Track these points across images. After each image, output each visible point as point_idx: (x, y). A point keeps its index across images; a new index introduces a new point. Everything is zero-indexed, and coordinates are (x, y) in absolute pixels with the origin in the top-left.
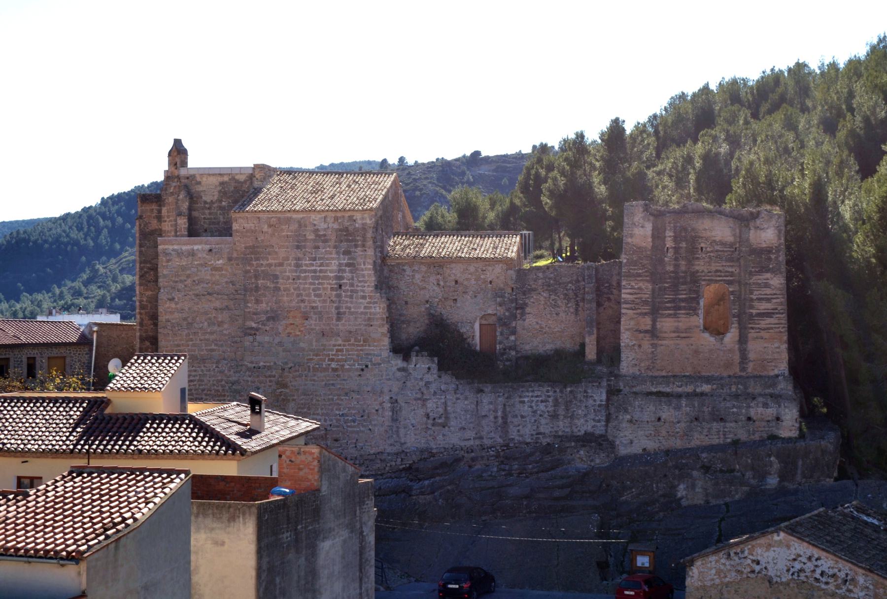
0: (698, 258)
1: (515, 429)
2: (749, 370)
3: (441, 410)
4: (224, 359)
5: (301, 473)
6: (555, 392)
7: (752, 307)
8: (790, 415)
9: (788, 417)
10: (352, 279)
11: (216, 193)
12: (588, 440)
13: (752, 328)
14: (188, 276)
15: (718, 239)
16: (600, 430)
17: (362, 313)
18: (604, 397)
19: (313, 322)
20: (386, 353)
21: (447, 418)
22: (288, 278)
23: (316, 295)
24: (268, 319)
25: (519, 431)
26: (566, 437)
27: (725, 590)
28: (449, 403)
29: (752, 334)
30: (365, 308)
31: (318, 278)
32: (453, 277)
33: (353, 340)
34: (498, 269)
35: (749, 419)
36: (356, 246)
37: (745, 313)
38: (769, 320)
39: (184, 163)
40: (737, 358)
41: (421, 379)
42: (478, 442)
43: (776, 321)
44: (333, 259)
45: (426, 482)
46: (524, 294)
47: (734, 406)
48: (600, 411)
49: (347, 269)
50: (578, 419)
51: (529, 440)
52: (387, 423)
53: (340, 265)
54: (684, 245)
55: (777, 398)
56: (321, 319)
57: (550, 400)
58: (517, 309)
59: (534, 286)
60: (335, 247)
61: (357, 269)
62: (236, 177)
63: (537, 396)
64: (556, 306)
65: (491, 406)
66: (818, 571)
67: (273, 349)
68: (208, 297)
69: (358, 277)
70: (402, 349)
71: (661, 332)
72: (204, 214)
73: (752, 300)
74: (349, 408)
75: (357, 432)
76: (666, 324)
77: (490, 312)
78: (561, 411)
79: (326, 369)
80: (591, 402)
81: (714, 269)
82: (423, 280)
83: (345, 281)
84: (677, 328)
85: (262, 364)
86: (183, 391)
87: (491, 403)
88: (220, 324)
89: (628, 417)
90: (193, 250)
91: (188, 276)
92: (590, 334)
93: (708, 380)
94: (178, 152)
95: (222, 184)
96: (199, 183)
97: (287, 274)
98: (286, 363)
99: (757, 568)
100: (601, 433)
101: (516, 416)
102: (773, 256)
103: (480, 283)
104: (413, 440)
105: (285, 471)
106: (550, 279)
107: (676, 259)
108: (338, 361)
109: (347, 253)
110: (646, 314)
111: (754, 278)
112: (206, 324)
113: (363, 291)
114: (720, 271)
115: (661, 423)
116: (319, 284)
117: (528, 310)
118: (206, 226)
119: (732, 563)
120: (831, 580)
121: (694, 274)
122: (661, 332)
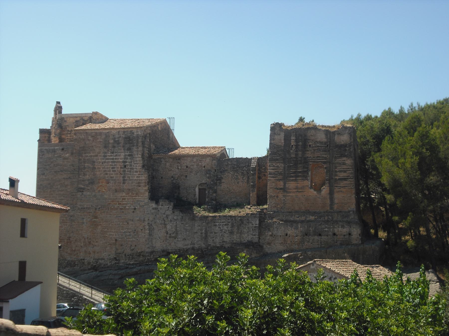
0: (308, 150)
2: (335, 209)
6: (232, 220)
7: (336, 175)
8: (356, 231)
10: (131, 162)
15: (318, 140)
16: (256, 240)
17: (135, 180)
18: (258, 222)
20: (147, 200)
21: (177, 234)
23: (113, 171)
24: (89, 184)
25: (213, 240)
26: (238, 244)
28: (178, 226)
29: (336, 189)
30: (137, 177)
33: (130, 193)
34: (208, 160)
35: (334, 234)
36: (133, 146)
37: (332, 179)
38: (345, 182)
39: (60, 112)
40: (328, 202)
41: (164, 214)
42: (192, 246)
43: (349, 183)
44: (122, 152)
46: (221, 172)
47: (326, 228)
49: (129, 157)
50: (244, 234)
51: (218, 245)
52: (146, 237)
53: (125, 155)
54: (300, 143)
55: (349, 223)
57: (230, 224)
58: (217, 180)
59: (226, 169)
60: (123, 147)
61: (134, 157)
62: (84, 118)
63: (223, 222)
65: (199, 228)
69: (134, 161)
70: (154, 197)
71: (289, 189)
72: (67, 136)
73: (336, 172)
76: (291, 185)
77: (203, 182)
78: (235, 230)
80: (251, 225)
81: (316, 156)
83: (128, 164)
87: (199, 226)
89: (270, 233)
92: (253, 191)
93: (314, 214)
94: (58, 108)
97: (99, 160)
100: (255, 241)
101: (212, 233)
102: (347, 149)
106: (234, 165)
107: (296, 151)
108: (123, 204)
109: (129, 149)
110: (280, 180)
111: (337, 160)
112: (59, 186)
114: (319, 157)
115: (288, 237)
117: (223, 181)
122: (289, 189)
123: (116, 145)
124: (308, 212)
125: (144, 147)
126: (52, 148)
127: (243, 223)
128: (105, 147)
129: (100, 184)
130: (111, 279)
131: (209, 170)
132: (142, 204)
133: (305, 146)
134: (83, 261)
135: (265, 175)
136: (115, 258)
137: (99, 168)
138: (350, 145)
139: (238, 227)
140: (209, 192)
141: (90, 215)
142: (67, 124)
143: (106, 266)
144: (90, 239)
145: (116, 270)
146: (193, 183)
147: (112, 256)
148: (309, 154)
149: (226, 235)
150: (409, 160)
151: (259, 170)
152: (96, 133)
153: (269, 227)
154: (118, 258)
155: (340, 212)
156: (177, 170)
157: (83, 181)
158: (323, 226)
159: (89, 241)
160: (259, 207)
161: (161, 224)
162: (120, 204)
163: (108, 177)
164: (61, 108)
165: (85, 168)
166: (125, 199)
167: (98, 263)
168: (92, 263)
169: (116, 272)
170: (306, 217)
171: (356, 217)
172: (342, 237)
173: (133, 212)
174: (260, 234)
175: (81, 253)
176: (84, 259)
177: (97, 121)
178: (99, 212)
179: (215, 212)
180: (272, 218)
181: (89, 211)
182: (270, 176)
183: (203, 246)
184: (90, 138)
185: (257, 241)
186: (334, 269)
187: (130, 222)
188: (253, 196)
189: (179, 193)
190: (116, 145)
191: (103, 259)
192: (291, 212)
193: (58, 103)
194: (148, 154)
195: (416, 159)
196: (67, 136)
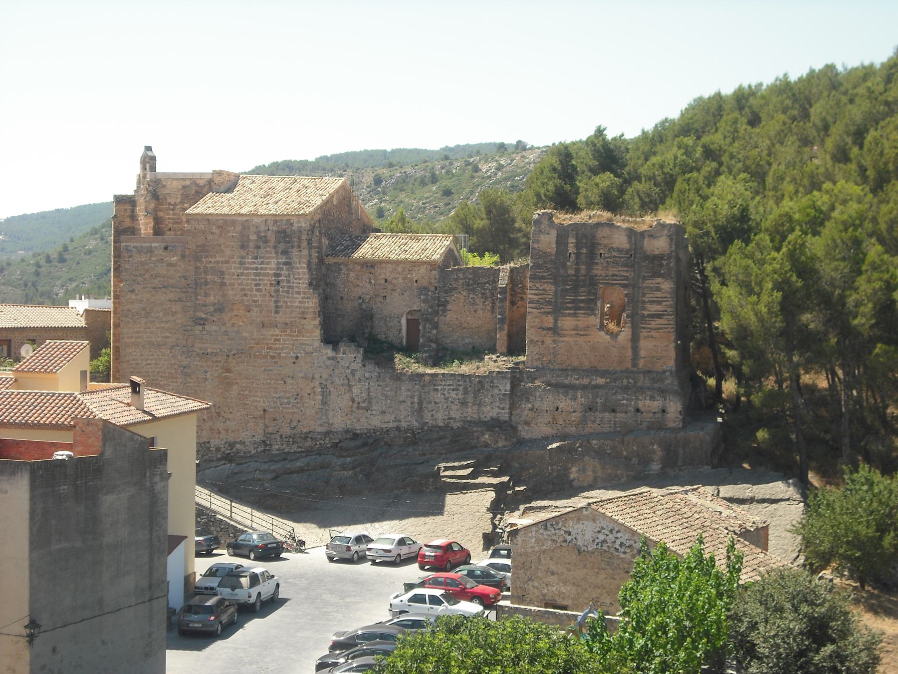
0: (597, 263)
1: (429, 414)
2: (641, 366)
3: (364, 395)
4: (177, 346)
5: (90, 441)
7: (644, 309)
8: (674, 408)
9: (673, 410)
10: (289, 276)
11: (179, 196)
12: (495, 425)
13: (644, 328)
14: (147, 271)
15: (615, 246)
16: (505, 416)
17: (297, 307)
18: (508, 387)
19: (255, 312)
20: (317, 343)
21: (370, 402)
22: (234, 274)
23: (257, 290)
24: (215, 311)
25: (432, 416)
26: (474, 422)
27: (542, 556)
28: (372, 390)
29: (644, 333)
30: (300, 302)
31: (258, 275)
32: (383, 276)
33: (289, 331)
34: (423, 270)
35: (638, 410)
36: (293, 247)
37: (637, 314)
38: (659, 321)
39: (153, 168)
40: (629, 353)
41: (348, 367)
42: (396, 424)
43: (666, 322)
44: (272, 258)
45: (349, 459)
46: (446, 292)
47: (624, 399)
48: (504, 400)
49: (285, 267)
51: (441, 424)
52: (318, 406)
53: (278, 263)
54: (584, 251)
55: (663, 392)
56: (261, 312)
57: (461, 388)
58: (439, 306)
60: (275, 247)
61: (293, 268)
62: (197, 182)
64: (474, 304)
65: (409, 393)
66: (618, 542)
67: (220, 338)
68: (163, 290)
69: (294, 275)
70: (330, 339)
72: (169, 214)
73: (644, 302)
74: (285, 392)
75: (292, 413)
76: (567, 322)
77: (415, 308)
78: (470, 398)
79: (265, 357)
80: (496, 391)
81: (611, 273)
82: (357, 278)
83: (282, 278)
84: (577, 326)
85: (209, 350)
86: (83, 374)
87: (409, 390)
88: (174, 314)
89: (530, 406)
90: (151, 247)
91: (147, 271)
92: (501, 329)
93: (603, 374)
94: (149, 161)
95: (184, 187)
96: (165, 186)
97: (233, 270)
98: (231, 350)
99: (569, 538)
101: (430, 402)
102: (665, 263)
103: (407, 281)
104: (339, 421)
105: (78, 438)
106: (470, 279)
107: (577, 264)
108: (276, 349)
109: (285, 252)
110: (549, 313)
111: (647, 282)
112: (161, 314)
113: (299, 288)
114: (616, 275)
116: (260, 280)
117: (449, 307)
118: (170, 225)
119: (549, 533)
120: (628, 550)
121: (592, 278)
122: (562, 330)
123: (261, 244)
124: (594, 371)
125: (310, 248)
126: (147, 245)
127: (483, 387)
128: (243, 247)
129: (235, 313)
130: (259, 480)
131: (425, 288)
132: (309, 349)
133: (592, 255)
134: (207, 445)
135: (522, 298)
136: (264, 441)
137: (232, 284)
138: (669, 257)
139: (475, 394)
140: (424, 328)
141: (217, 366)
142: (167, 192)
143: (249, 455)
144: (219, 407)
145: (266, 462)
146: (397, 311)
147: (258, 438)
148: (598, 271)
149: (454, 407)
150: (765, 298)
151: (512, 289)
152: (226, 221)
153: (527, 395)
154: (268, 442)
155: (649, 372)
156: (368, 286)
157: (204, 306)
158: (619, 397)
159: (218, 411)
160: (511, 359)
161: (343, 385)
162: (270, 348)
163: (248, 300)
164: (154, 158)
165: (206, 283)
166: (279, 340)
167: (234, 450)
168: (223, 450)
169: (266, 466)
170: (592, 379)
171: (676, 383)
172: (651, 415)
173: (294, 363)
174: (512, 407)
175: (204, 432)
176: (209, 442)
177: (223, 188)
178: (234, 361)
179: (434, 365)
180: (533, 380)
181: (215, 359)
182: (531, 305)
183: (416, 424)
184: (214, 229)
185: (507, 419)
186: (617, 518)
187: (289, 381)
188: (501, 338)
189: (372, 328)
190: (261, 244)
191: (241, 443)
192: (566, 370)
193: (148, 148)
194: (317, 257)
195: (778, 295)
196: (169, 214)
